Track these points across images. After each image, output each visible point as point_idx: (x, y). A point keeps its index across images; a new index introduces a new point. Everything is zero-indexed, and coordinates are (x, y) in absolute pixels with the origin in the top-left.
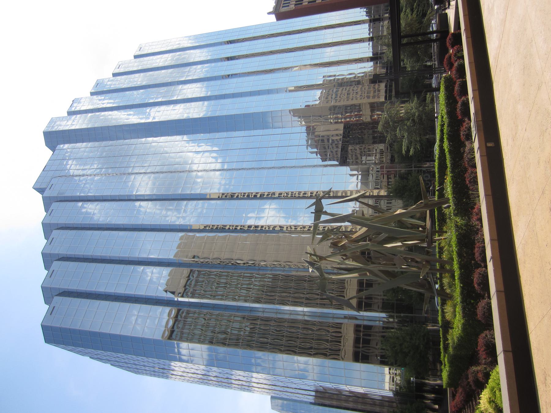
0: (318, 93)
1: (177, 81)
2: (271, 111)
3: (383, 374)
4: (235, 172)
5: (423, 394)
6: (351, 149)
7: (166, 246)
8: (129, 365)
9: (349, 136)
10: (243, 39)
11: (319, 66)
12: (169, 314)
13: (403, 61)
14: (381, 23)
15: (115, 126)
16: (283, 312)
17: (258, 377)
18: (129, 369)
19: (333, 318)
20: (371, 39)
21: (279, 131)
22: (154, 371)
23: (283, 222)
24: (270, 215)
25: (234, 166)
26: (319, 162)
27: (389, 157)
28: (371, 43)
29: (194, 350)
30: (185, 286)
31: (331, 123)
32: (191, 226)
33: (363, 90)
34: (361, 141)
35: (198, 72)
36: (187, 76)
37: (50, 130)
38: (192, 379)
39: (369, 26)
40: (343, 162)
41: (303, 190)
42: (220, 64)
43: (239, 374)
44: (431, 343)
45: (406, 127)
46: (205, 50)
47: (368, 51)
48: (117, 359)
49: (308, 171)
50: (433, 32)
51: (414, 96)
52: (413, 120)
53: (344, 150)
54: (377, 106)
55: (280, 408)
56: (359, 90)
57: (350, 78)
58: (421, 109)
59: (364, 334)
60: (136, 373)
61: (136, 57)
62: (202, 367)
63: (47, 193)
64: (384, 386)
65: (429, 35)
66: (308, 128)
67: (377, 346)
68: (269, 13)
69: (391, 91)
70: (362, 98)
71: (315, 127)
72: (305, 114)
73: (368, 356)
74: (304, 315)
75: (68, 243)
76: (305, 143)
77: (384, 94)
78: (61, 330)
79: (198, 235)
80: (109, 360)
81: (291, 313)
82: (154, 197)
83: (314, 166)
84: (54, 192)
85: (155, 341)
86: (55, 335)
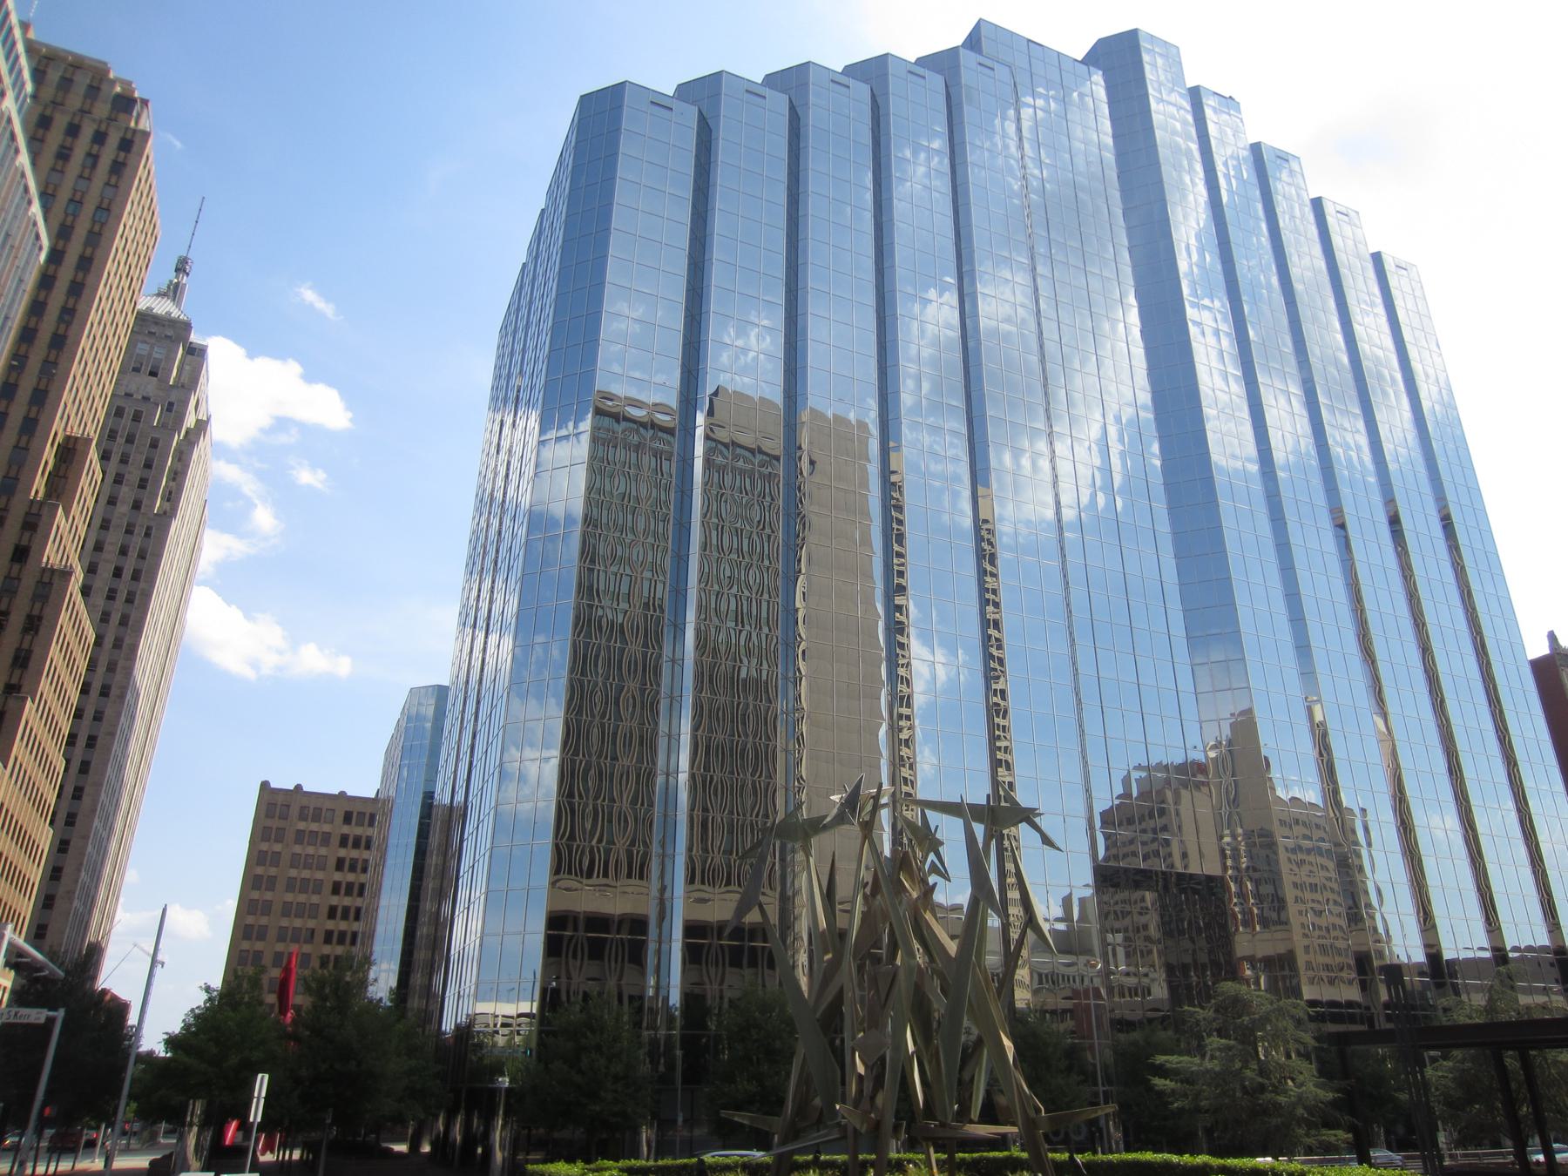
0: (1313, 795)
1: (1312, 380)
2: (1244, 659)
3: (513, 995)
4: (1055, 564)
5: (462, 1111)
6: (1143, 900)
7: (839, 389)
8: (524, 311)
9: (1183, 891)
10: (1463, 567)
11: (1394, 797)
12: (657, 407)
13: (1445, 1058)
14: (1556, 987)
15: (1168, 220)
16: (675, 714)
17: (502, 649)
18: (514, 309)
19: (663, 856)
20: (1500, 955)
21: (1186, 683)
22: (509, 376)
23: (919, 700)
24: (936, 666)
25: (1074, 559)
26: (1103, 802)
27: (1129, 1015)
28: (1487, 955)
29: (562, 472)
30: (733, 443)
31: (1221, 838)
32: (898, 448)
33: (1333, 934)
34: (1171, 929)
35: (1347, 437)
36: (1332, 409)
37: (1144, 44)
38: (490, 475)
39: (1543, 949)
40: (1106, 877)
41: (1017, 759)
42: (1377, 499)
43: (508, 604)
44: (604, 1136)
45: (1238, 1065)
46: (1412, 436)
47: (1460, 946)
48: (540, 279)
49: (1074, 774)
50: (1549, 1153)
51: (1338, 1091)
52: (1262, 1088)
53: (1141, 879)
54: (1284, 978)
55: (414, 711)
56: (1332, 919)
57: (1366, 892)
58: (1300, 1111)
59: (624, 941)
60: (504, 327)
61: (1377, 258)
62: (525, 501)
63: (968, 59)
64: (483, 1000)
65: (1537, 1140)
66: (1200, 768)
67: (582, 975)
68: (1552, 637)
69: (1336, 1018)
70: (1307, 926)
71: (1205, 789)
72: (1242, 754)
73: (559, 955)
74: (668, 775)
75: (838, 127)
76: (1153, 762)
77: (1326, 998)
78: (615, 131)
79: (874, 469)
80: (536, 258)
81: (673, 738)
82: (971, 344)
83: (1088, 791)
84: (973, 72)
85: (590, 376)
86: (602, 118)
